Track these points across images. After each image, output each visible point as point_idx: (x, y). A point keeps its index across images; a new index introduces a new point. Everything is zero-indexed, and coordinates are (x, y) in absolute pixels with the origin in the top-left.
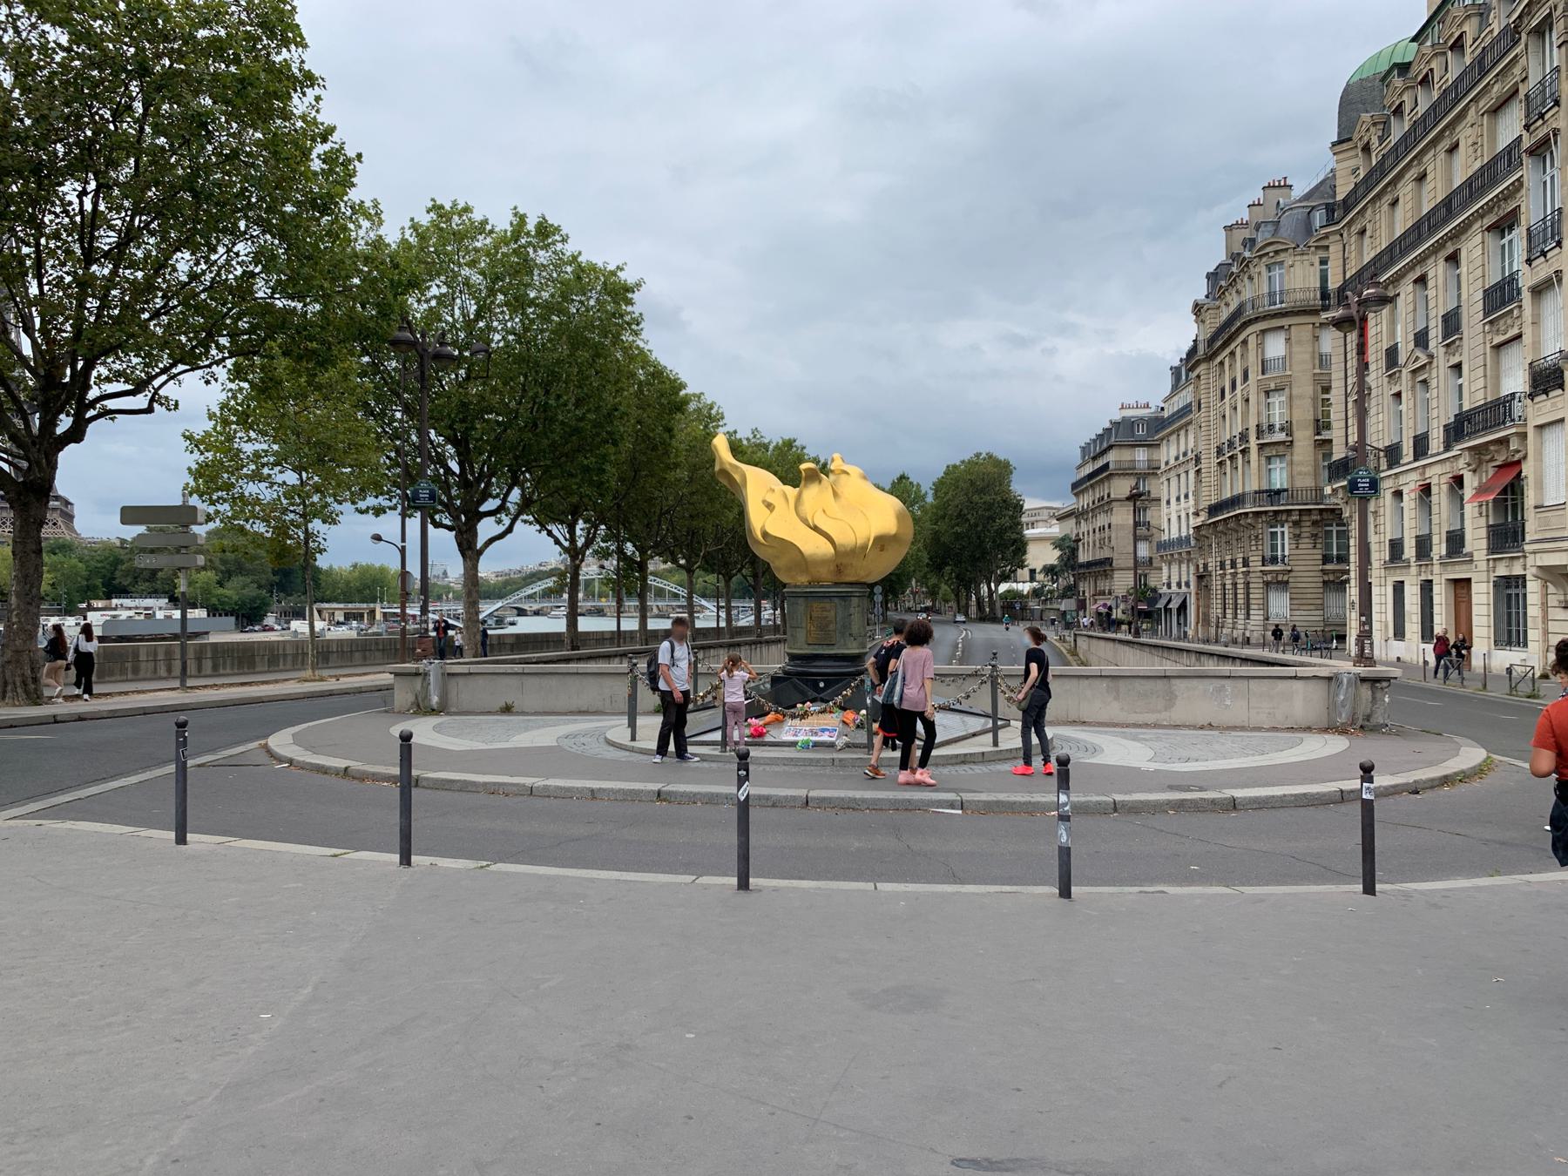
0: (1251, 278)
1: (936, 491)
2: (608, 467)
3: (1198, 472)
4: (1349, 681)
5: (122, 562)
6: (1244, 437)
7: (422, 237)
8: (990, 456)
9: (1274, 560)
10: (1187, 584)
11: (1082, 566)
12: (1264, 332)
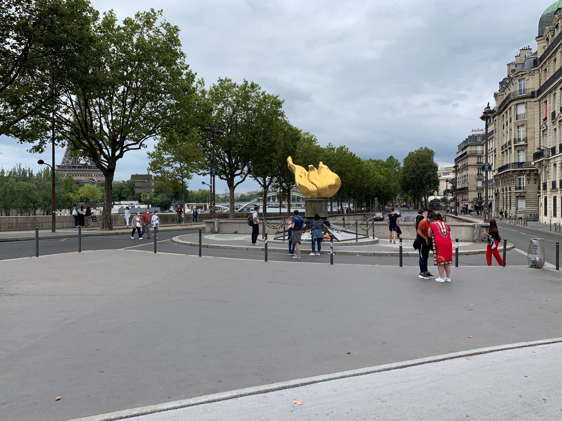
0: (513, 84)
1: (405, 162)
2: (273, 160)
3: (495, 155)
4: (478, 227)
5: (124, 189)
6: (510, 143)
7: (216, 90)
8: (426, 148)
9: (520, 188)
10: (492, 197)
11: (458, 190)
12: (517, 104)
